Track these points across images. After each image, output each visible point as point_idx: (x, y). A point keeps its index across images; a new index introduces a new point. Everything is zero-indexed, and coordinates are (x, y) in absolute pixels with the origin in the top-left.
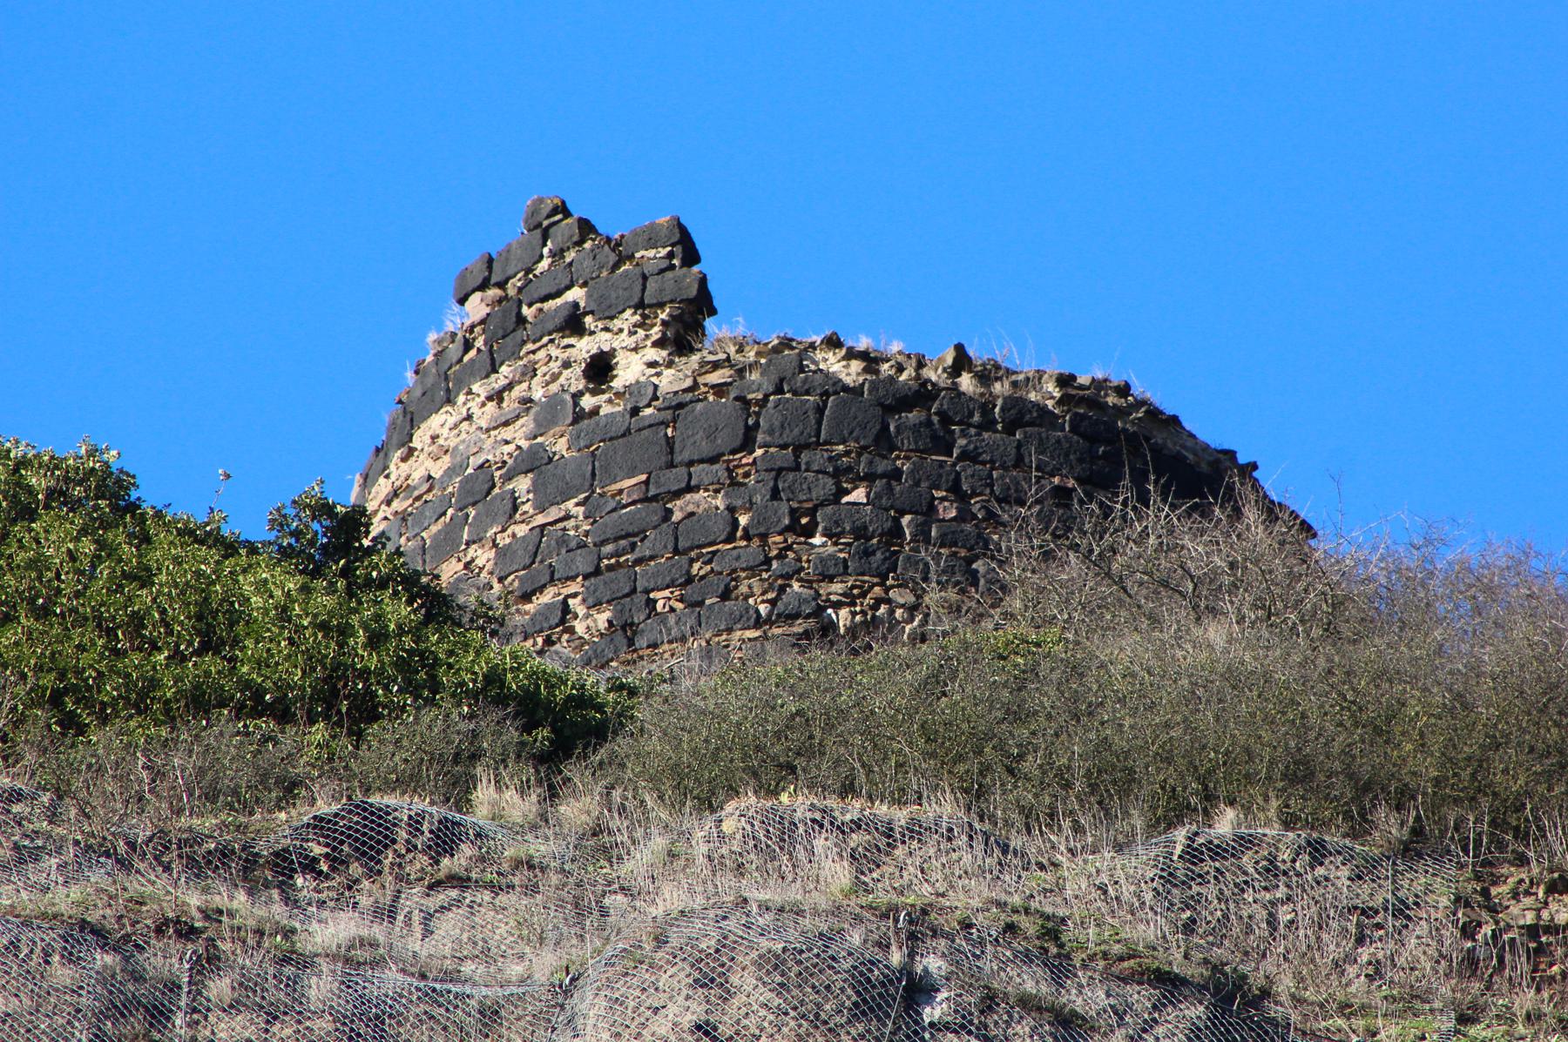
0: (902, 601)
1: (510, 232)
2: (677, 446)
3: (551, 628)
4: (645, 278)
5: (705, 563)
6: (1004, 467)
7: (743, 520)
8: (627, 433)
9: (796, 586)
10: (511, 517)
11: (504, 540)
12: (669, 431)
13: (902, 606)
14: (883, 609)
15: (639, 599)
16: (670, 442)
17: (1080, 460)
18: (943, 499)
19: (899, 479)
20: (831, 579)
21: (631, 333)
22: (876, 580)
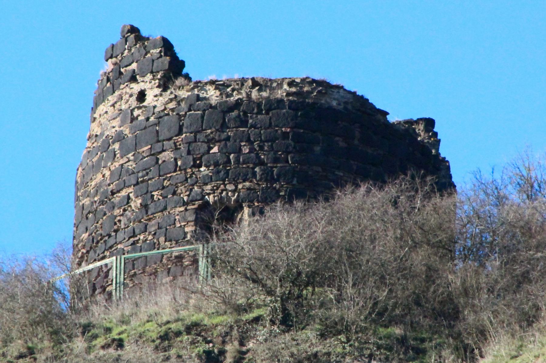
0: (230, 189)
1: (116, 38)
2: (159, 134)
3: (125, 206)
4: (153, 61)
5: (168, 181)
6: (265, 129)
7: (179, 163)
8: (145, 128)
10: (114, 159)
11: (113, 168)
12: (157, 128)
13: (230, 191)
14: (224, 193)
15: (149, 195)
16: (157, 132)
17: (292, 120)
18: (244, 145)
21: (150, 82)
22: (221, 182)
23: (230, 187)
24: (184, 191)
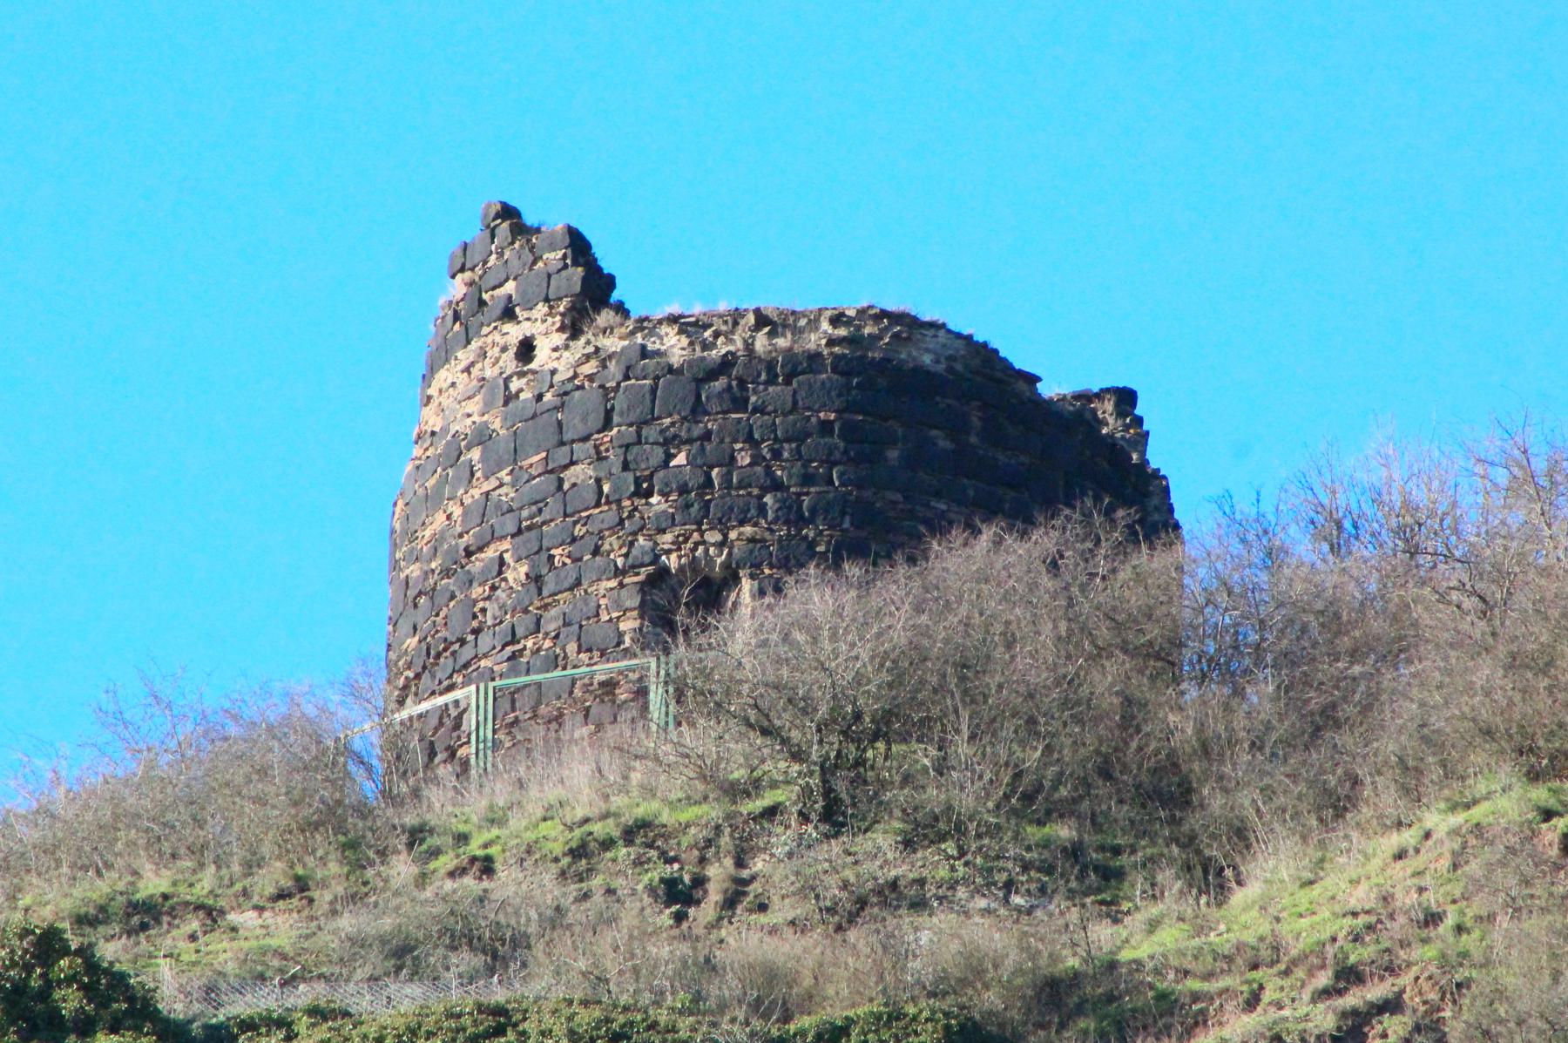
1: (473, 230)
4: (549, 276)
6: (785, 415)
7: (606, 488)
8: (534, 416)
9: (641, 539)
14: (701, 549)
15: (544, 556)
16: (560, 424)
17: (839, 395)
19: (709, 439)
20: (663, 531)
21: (544, 321)
23: (713, 537)
24: (616, 547)
